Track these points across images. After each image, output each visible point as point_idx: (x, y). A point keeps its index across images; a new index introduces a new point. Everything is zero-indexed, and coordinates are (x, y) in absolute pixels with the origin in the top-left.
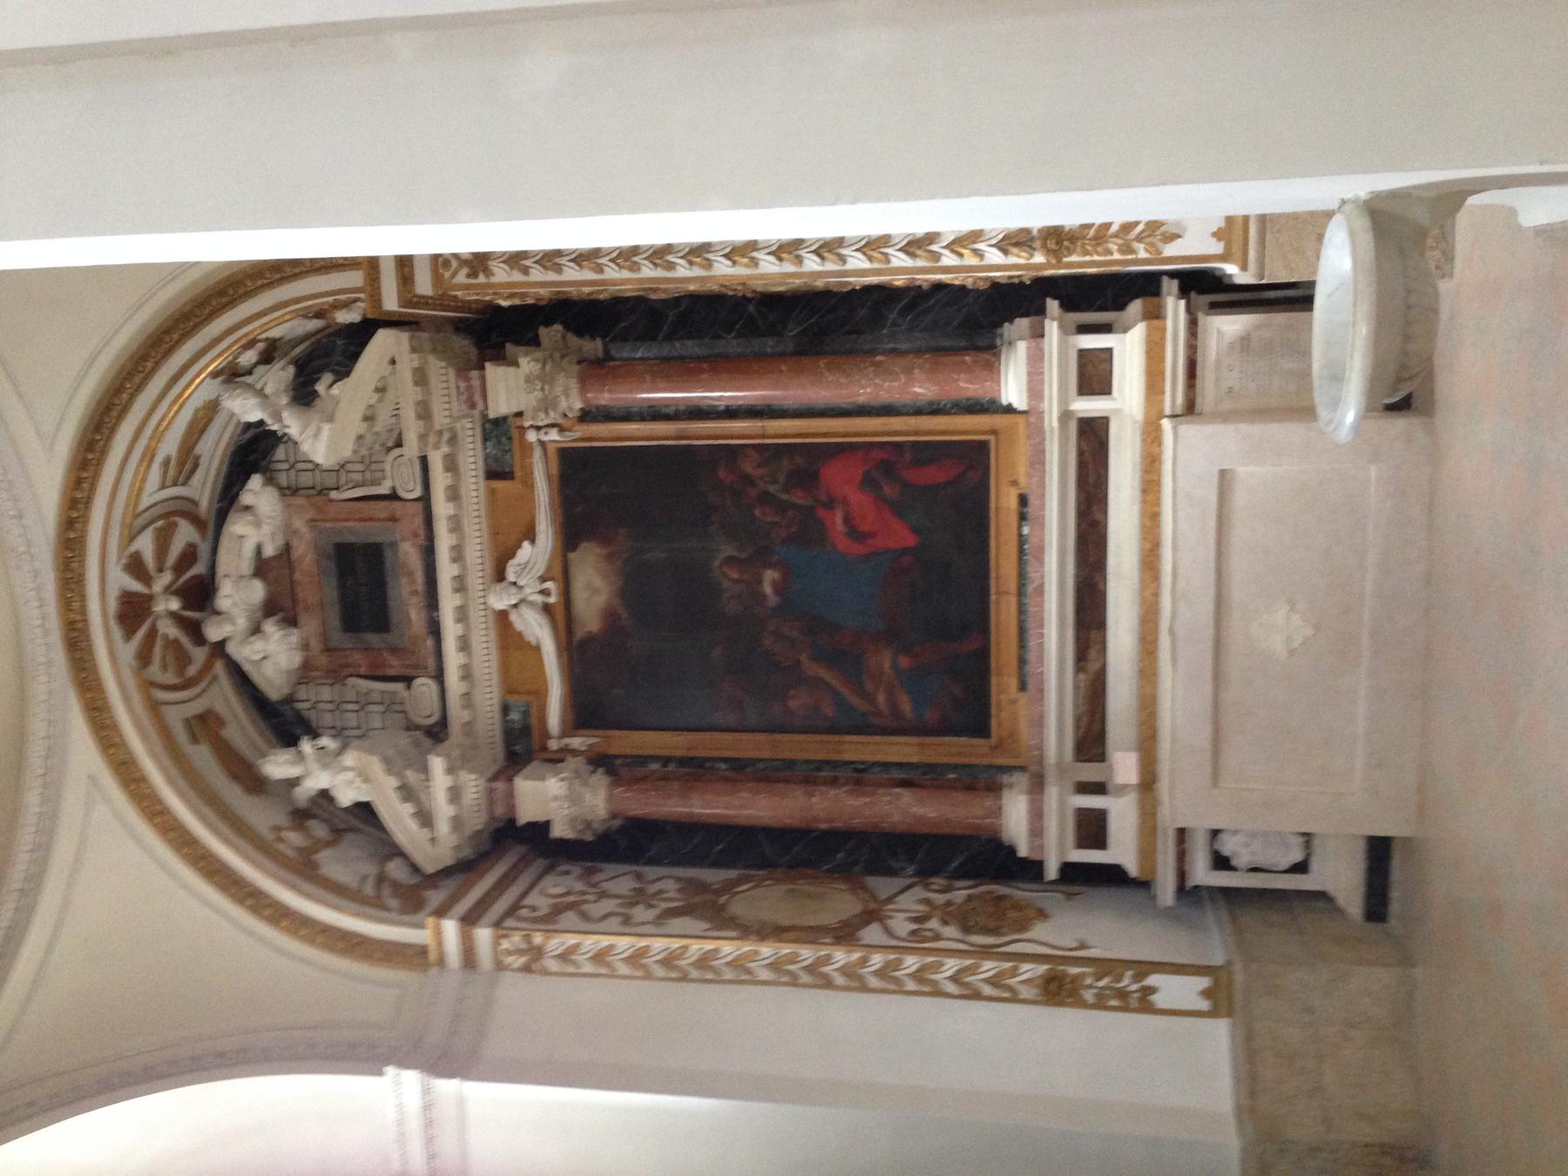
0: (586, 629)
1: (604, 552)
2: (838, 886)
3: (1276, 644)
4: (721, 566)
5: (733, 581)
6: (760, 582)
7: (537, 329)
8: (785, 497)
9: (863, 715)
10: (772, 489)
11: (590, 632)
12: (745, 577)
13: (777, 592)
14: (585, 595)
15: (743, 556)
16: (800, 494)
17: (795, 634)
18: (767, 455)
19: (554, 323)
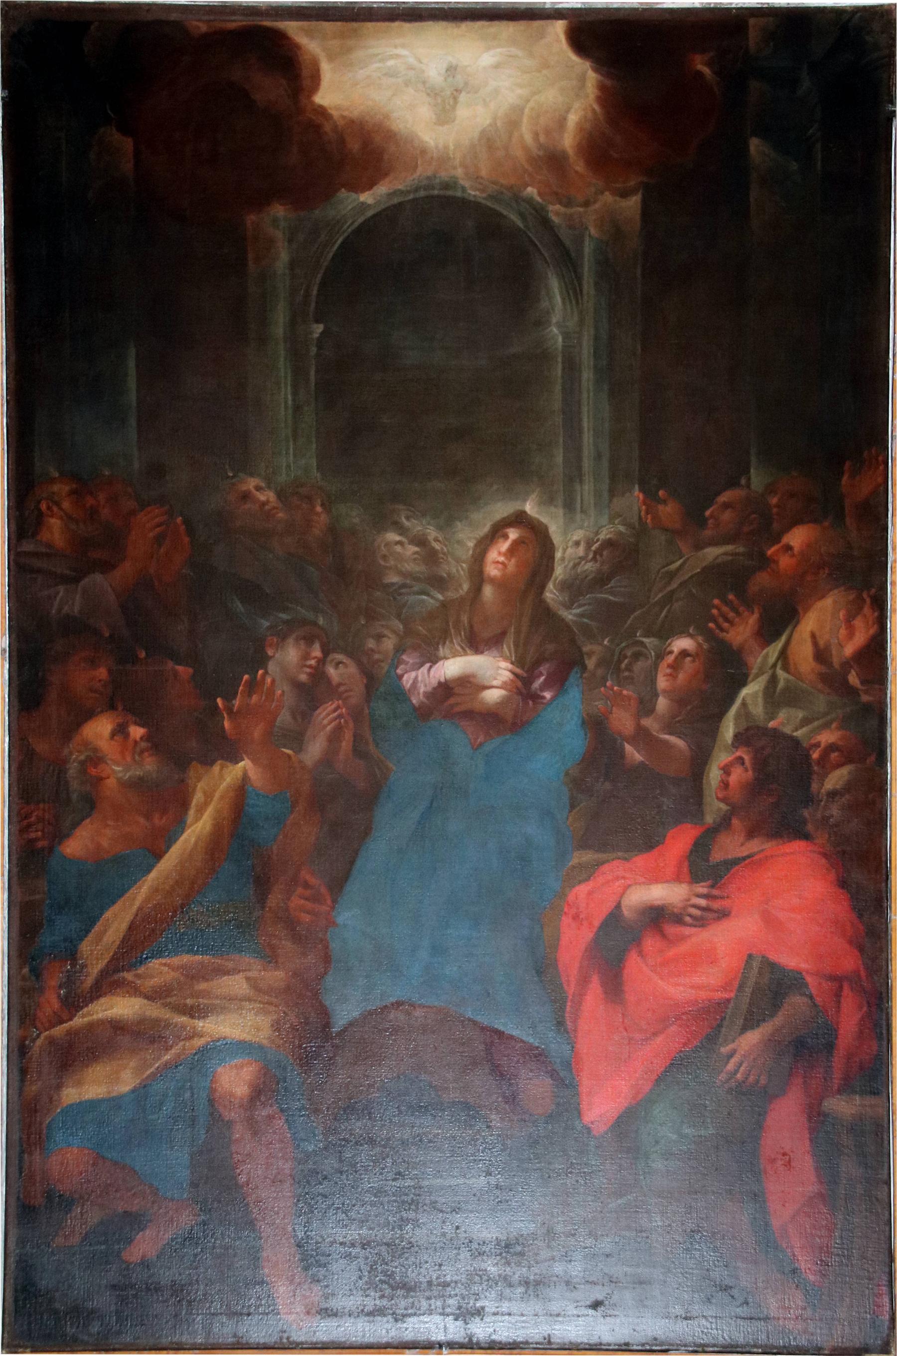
0: (326, 68)
1: (568, 141)
2: (289, 378)
3: (795, 168)
4: (519, 519)
5: (479, 558)
6: (475, 644)
7: (312, 103)
8: (729, 729)
9: (72, 955)
10: (752, 690)
11: (316, 78)
12: (488, 591)
13: (446, 689)
14: (434, 72)
15: (551, 594)
16: (737, 776)
17: (315, 750)
18: (853, 679)
19: (205, 35)
